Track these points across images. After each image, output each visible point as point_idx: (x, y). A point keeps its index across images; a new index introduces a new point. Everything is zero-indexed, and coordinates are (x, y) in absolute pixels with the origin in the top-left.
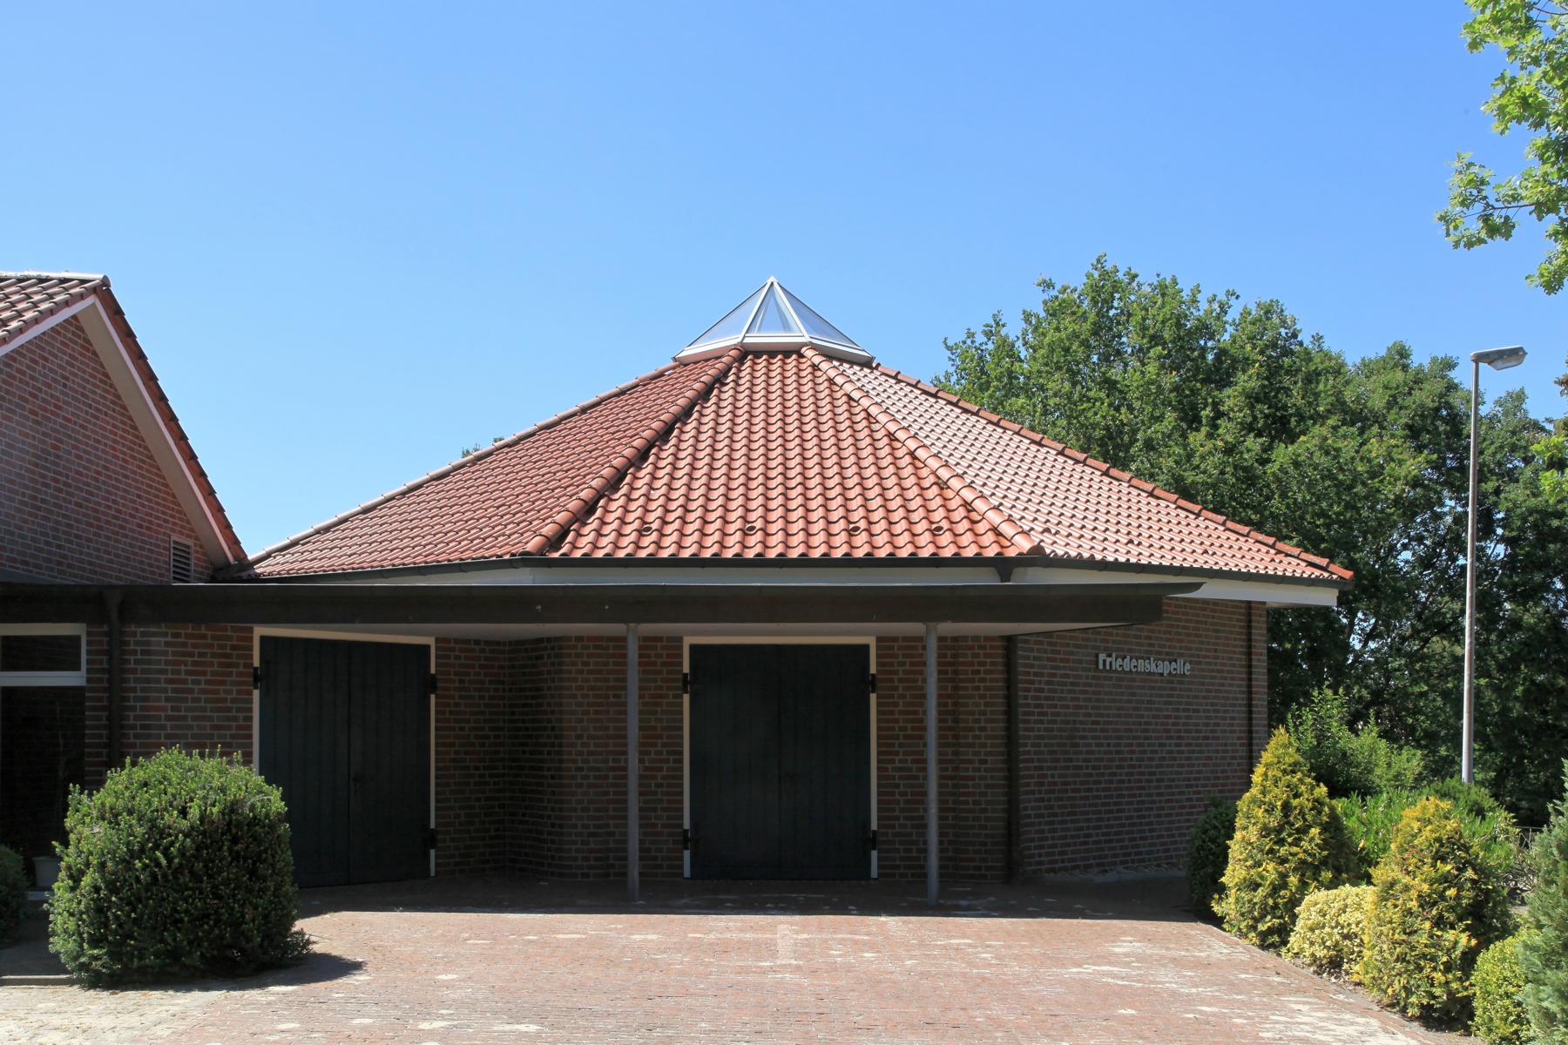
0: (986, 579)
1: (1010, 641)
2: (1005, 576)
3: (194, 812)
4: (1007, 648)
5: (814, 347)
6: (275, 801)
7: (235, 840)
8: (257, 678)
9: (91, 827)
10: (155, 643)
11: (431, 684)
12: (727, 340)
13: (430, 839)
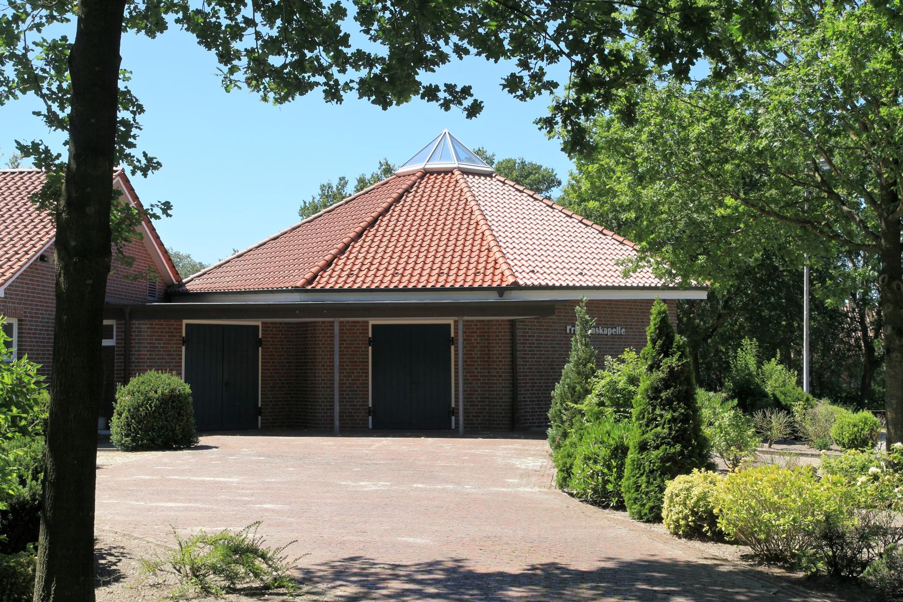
0: (492, 298)
1: (513, 323)
2: (501, 295)
3: (159, 392)
4: (512, 325)
5: (460, 169)
6: (187, 389)
7: (173, 402)
8: (184, 341)
9: (125, 398)
10: (143, 328)
11: (259, 342)
12: (418, 166)
13: (259, 412)
